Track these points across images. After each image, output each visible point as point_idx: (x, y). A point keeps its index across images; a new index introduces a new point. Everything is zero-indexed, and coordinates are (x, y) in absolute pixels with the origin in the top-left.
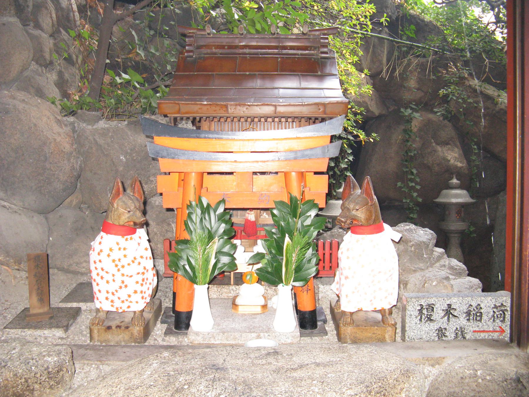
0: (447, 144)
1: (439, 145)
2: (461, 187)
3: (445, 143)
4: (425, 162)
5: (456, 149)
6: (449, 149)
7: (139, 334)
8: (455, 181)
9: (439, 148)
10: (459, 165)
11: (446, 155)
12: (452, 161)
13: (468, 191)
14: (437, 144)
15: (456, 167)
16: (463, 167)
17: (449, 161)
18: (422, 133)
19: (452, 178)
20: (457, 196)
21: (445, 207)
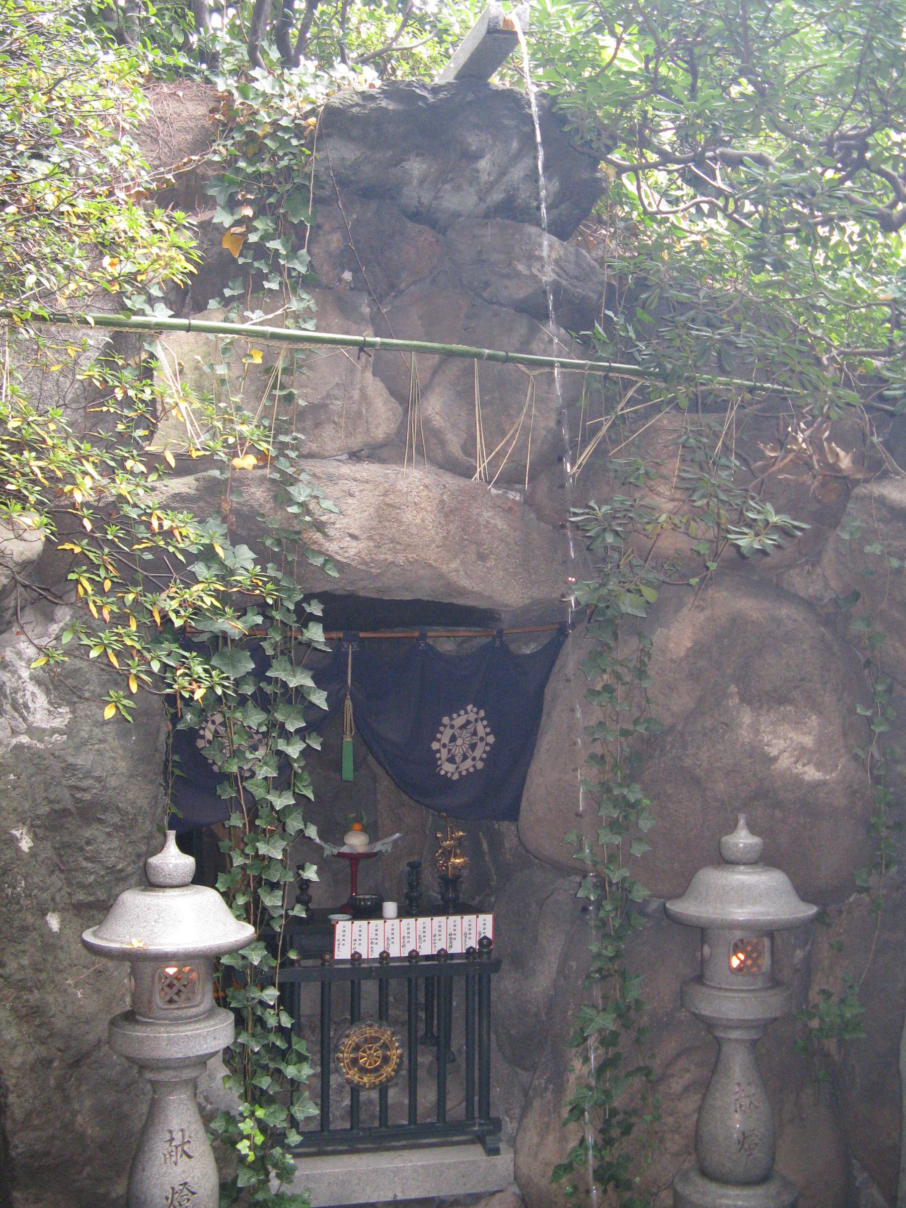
0: (783, 700)
1: (750, 703)
2: (765, 859)
3: (777, 698)
4: (688, 762)
5: (814, 720)
6: (784, 719)
7: (697, 248)
8: (743, 839)
9: (746, 717)
10: (812, 774)
11: (766, 738)
12: (785, 762)
13: (786, 871)
14: (746, 699)
15: (798, 781)
16: (825, 783)
17: (775, 759)
18: (701, 663)
19: (732, 828)
20: (745, 895)
21: (700, 932)
